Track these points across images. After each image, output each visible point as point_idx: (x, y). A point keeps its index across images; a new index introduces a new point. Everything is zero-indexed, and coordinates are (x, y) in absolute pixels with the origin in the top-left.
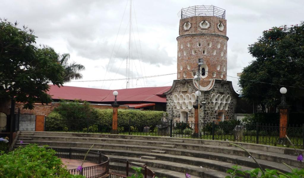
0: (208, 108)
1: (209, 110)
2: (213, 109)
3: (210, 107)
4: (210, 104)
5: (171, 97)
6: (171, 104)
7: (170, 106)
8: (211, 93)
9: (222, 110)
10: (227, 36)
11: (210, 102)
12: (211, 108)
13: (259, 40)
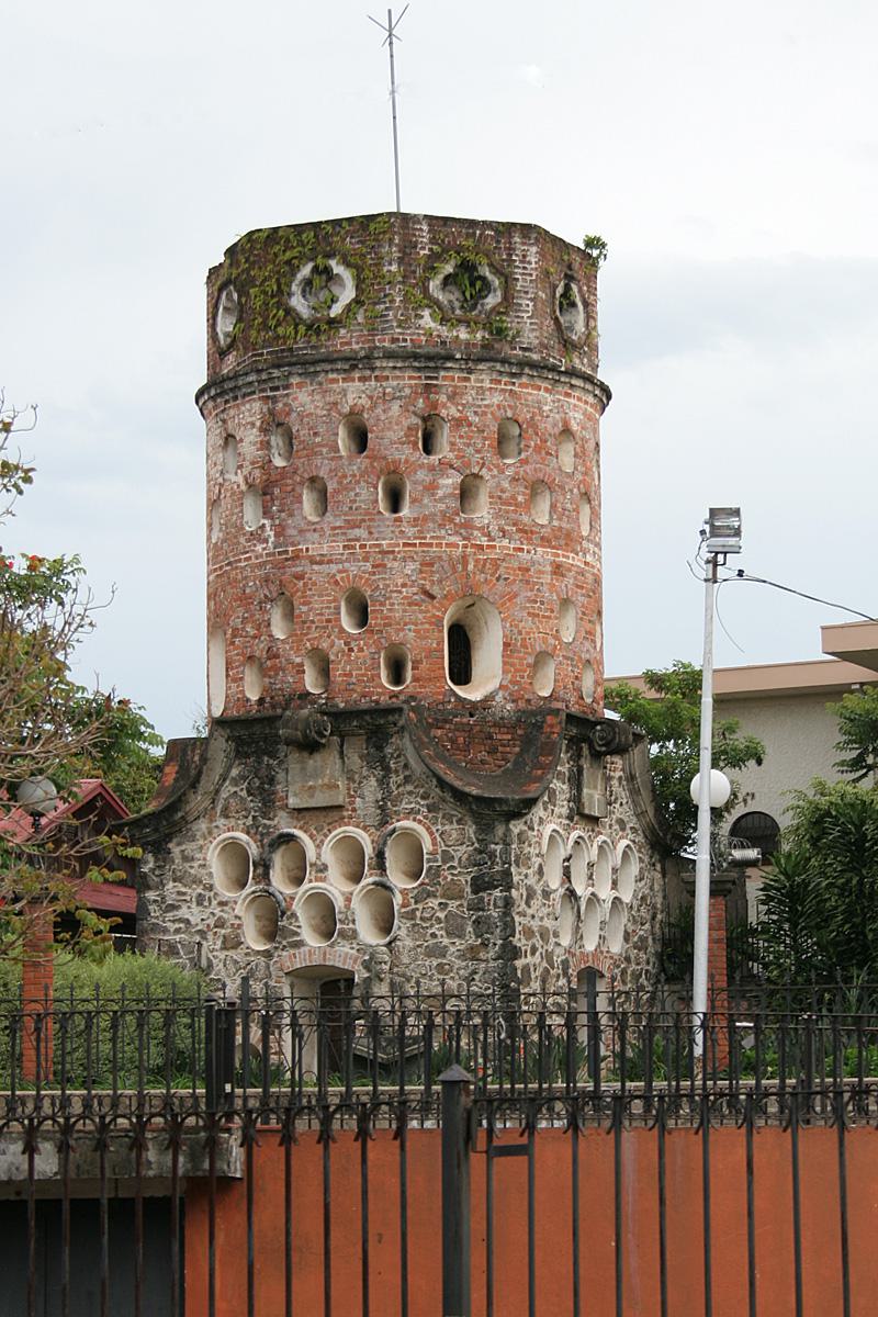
0: (529, 933)
1: (534, 950)
2: (552, 940)
3: (535, 924)
4: (536, 903)
5: (186, 859)
6: (183, 912)
7: (172, 927)
8: (541, 821)
9: (594, 954)
10: (601, 376)
11: (538, 889)
12: (544, 934)
13: (339, 903)
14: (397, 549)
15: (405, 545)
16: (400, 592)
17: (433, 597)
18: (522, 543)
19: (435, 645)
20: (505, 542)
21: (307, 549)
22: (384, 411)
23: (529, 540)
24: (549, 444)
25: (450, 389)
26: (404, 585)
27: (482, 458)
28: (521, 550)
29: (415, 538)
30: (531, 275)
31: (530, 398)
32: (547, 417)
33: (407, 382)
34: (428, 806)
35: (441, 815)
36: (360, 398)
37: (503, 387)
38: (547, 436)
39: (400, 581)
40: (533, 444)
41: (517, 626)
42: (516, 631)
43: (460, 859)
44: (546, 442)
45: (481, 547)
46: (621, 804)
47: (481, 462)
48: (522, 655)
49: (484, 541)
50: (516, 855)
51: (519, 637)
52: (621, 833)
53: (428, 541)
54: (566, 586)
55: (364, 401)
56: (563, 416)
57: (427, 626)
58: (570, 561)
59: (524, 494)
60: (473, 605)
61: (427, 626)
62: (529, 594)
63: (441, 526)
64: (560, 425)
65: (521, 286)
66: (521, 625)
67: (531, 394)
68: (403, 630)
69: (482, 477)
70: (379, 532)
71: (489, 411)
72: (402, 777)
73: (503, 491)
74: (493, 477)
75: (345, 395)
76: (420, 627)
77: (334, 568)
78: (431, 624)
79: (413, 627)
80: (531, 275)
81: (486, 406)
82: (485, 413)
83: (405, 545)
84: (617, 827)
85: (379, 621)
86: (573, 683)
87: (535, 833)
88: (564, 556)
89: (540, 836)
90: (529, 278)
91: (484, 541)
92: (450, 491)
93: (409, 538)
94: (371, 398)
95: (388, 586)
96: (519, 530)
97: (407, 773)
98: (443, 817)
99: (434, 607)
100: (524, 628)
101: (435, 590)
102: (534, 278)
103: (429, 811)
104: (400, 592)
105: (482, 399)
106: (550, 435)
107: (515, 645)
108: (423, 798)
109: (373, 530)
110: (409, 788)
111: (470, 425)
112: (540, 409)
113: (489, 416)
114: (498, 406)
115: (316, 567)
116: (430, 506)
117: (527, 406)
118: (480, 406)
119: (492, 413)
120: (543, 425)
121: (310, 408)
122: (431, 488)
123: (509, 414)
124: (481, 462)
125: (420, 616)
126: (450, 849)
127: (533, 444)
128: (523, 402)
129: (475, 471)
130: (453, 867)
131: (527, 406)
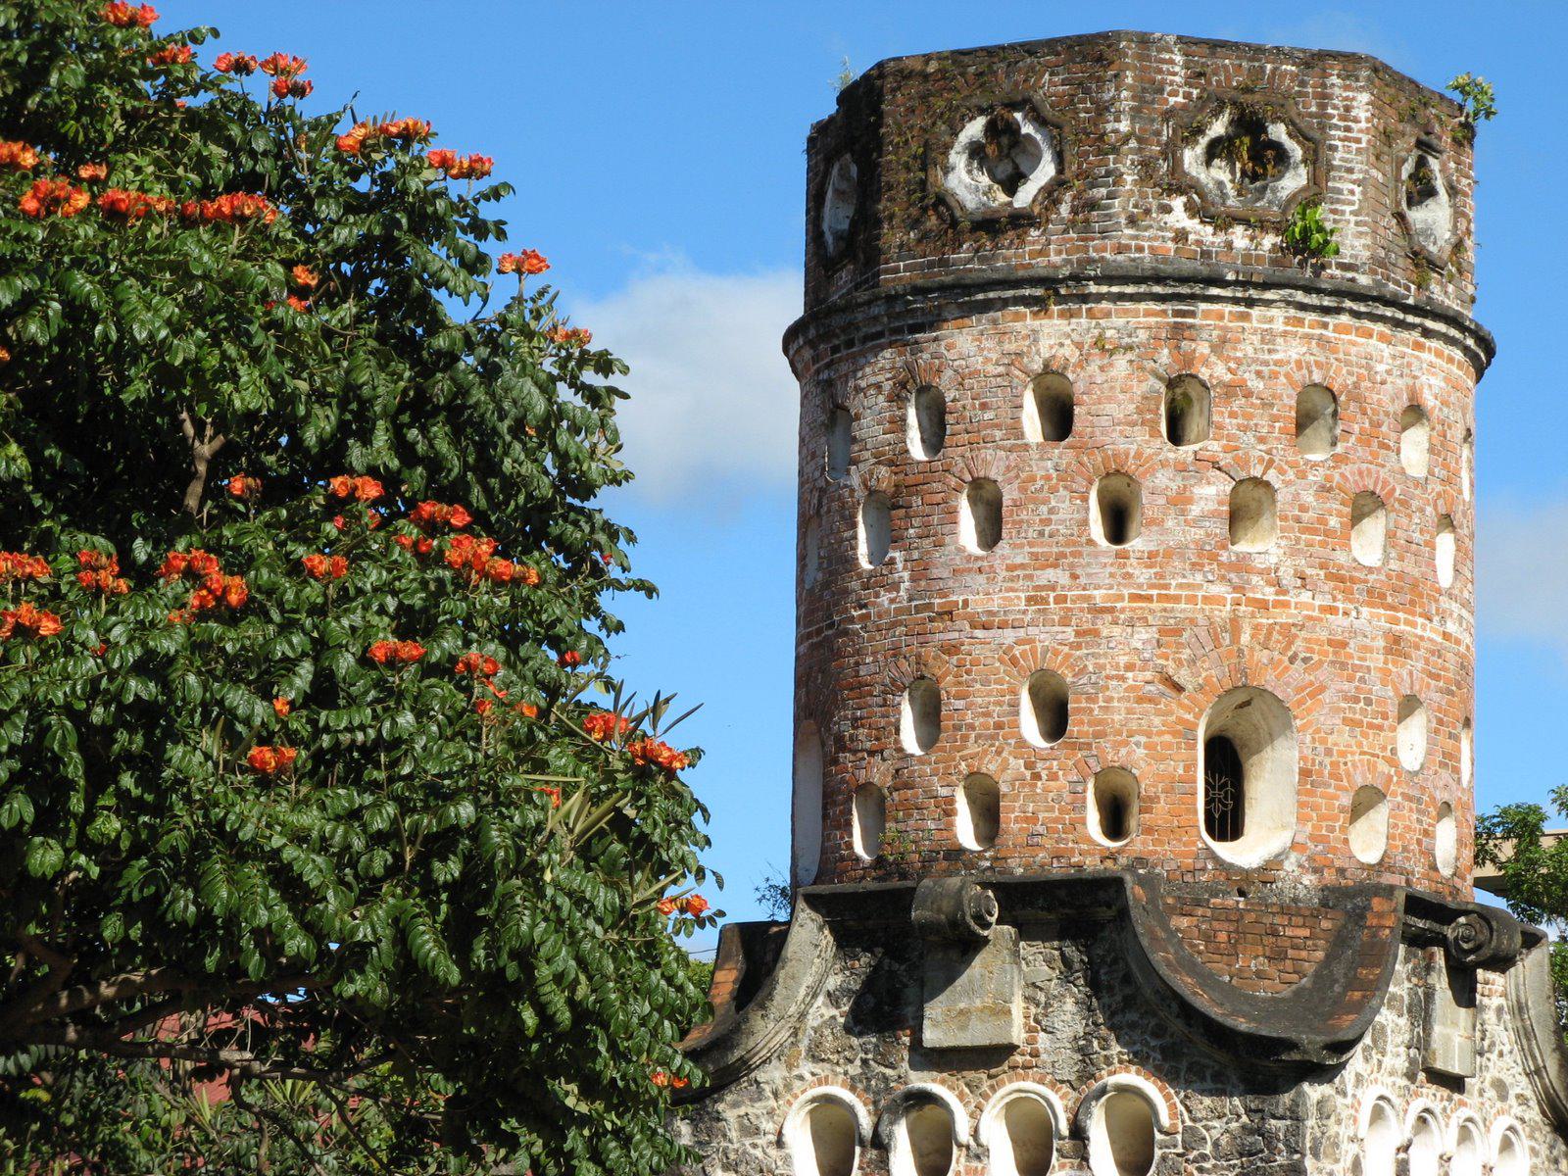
14: (1119, 605)
15: (1135, 598)
16: (1123, 679)
17: (1179, 688)
18: (1335, 599)
19: (1181, 772)
20: (1306, 596)
21: (966, 603)
22: (1102, 369)
23: (1348, 593)
24: (1384, 428)
25: (1215, 333)
26: (1130, 667)
27: (1269, 452)
28: (1333, 610)
29: (1152, 586)
30: (1358, 141)
31: (1353, 350)
32: (1383, 383)
33: (1142, 319)
34: (1163, 1050)
35: (1184, 1065)
36: (1062, 345)
37: (1307, 330)
38: (1382, 416)
39: (1123, 660)
40: (1356, 428)
41: (1323, 741)
42: (1321, 749)
43: (1216, 1144)
44: (1379, 425)
45: (1263, 605)
46: (1501, 1054)
47: (1267, 457)
48: (1331, 790)
49: (1269, 594)
50: (1314, 1139)
51: (1327, 761)
52: (1499, 1104)
53: (1172, 592)
54: (1411, 674)
55: (1069, 352)
56: (1410, 382)
57: (1167, 738)
58: (1419, 631)
59: (1340, 514)
60: (1248, 703)
61: (1167, 738)
62: (1346, 686)
63: (1196, 566)
64: (1405, 396)
65: (1342, 159)
66: (1331, 739)
67: (1354, 344)
68: (1126, 744)
69: (1267, 484)
70: (1089, 575)
71: (1282, 370)
72: (1118, 998)
73: (1303, 509)
74: (1288, 483)
75: (1036, 341)
76: (1155, 739)
77: (1009, 636)
78: (1174, 734)
79: (1143, 739)
80: (1358, 141)
81: (1277, 363)
82: (1274, 375)
83: (1135, 598)
84: (1491, 1093)
85: (1086, 728)
86: (1419, 842)
87: (1349, 1100)
88: (1407, 622)
89: (1356, 1105)
90: (1354, 146)
91: (1269, 594)
92: (1212, 506)
93: (1140, 586)
94: (1079, 346)
95: (1103, 667)
96: (1330, 577)
97: (1128, 991)
98: (1189, 1069)
99: (1181, 705)
100: (1336, 744)
101: (1183, 676)
102: (1364, 145)
103: (1165, 1059)
104: (1123, 679)
105: (1270, 351)
106: (1387, 414)
107: (1320, 773)
108: (1155, 1035)
109: (1079, 572)
110: (1132, 1016)
111: (1248, 394)
112: (1369, 368)
113: (1283, 379)
114: (1299, 364)
115: (979, 633)
116: (1176, 531)
117: (1348, 363)
118: (1266, 363)
119: (1287, 376)
120: (1376, 397)
121: (977, 362)
122: (1180, 501)
123: (1317, 377)
124: (1267, 457)
125: (1157, 721)
126: (1199, 1125)
127: (1356, 428)
128: (1341, 356)
129: (1257, 472)
130: (1204, 1157)
131: (1348, 363)
